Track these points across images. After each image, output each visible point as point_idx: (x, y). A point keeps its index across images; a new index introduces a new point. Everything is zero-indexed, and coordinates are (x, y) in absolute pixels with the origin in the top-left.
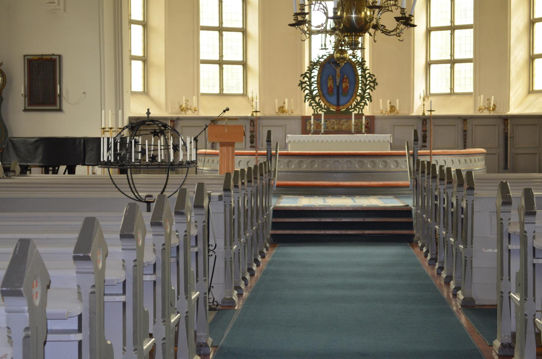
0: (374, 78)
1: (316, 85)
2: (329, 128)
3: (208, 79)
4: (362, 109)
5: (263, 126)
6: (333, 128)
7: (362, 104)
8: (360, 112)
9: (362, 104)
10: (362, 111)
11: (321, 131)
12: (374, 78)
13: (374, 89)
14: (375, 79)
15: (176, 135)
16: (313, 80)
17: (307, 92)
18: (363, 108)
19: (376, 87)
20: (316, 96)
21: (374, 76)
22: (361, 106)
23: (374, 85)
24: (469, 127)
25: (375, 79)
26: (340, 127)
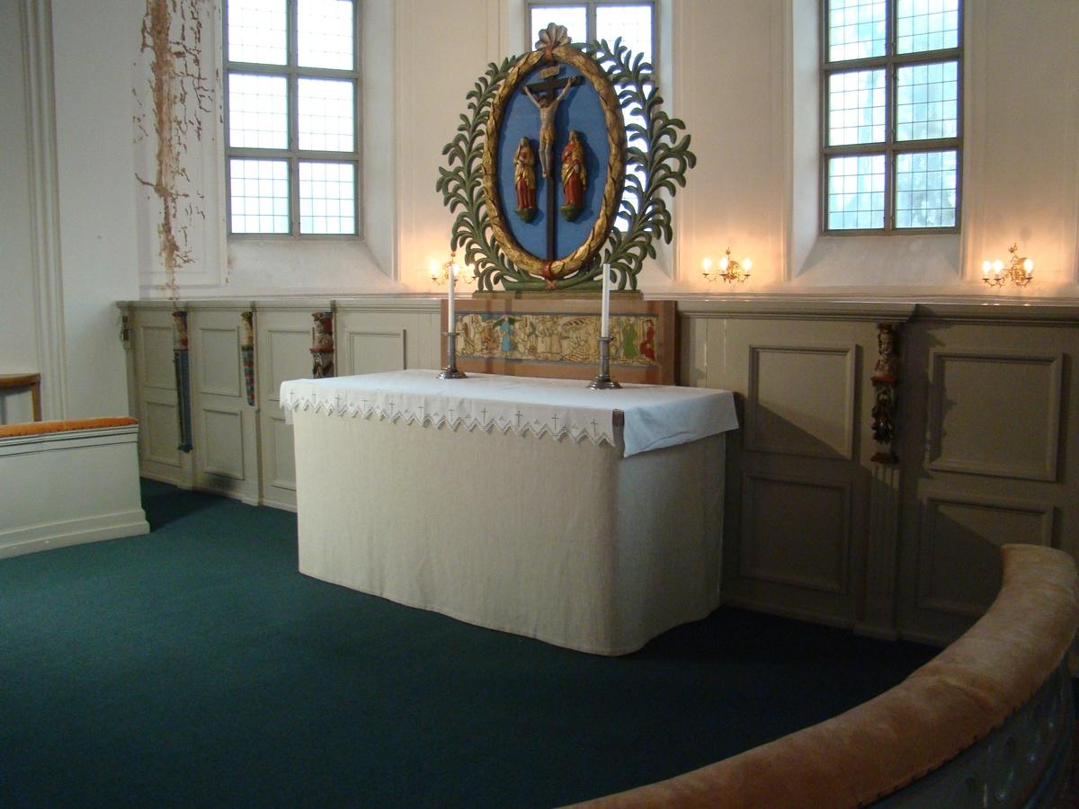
0: (681, 134)
1: (490, 109)
2: (521, 348)
3: (256, 199)
4: (633, 274)
5: (352, 334)
6: (533, 350)
7: (636, 251)
8: (628, 287)
9: (636, 251)
10: (634, 283)
11: (983, 804)
12: (681, 134)
13: (683, 182)
14: (688, 139)
15: (643, 345)
16: (477, 162)
17: (461, 208)
18: (639, 267)
19: (688, 174)
20: (481, 133)
21: (681, 125)
22: (630, 258)
23: (683, 169)
24: (196, 336)
25: (688, 139)
26: (555, 348)
